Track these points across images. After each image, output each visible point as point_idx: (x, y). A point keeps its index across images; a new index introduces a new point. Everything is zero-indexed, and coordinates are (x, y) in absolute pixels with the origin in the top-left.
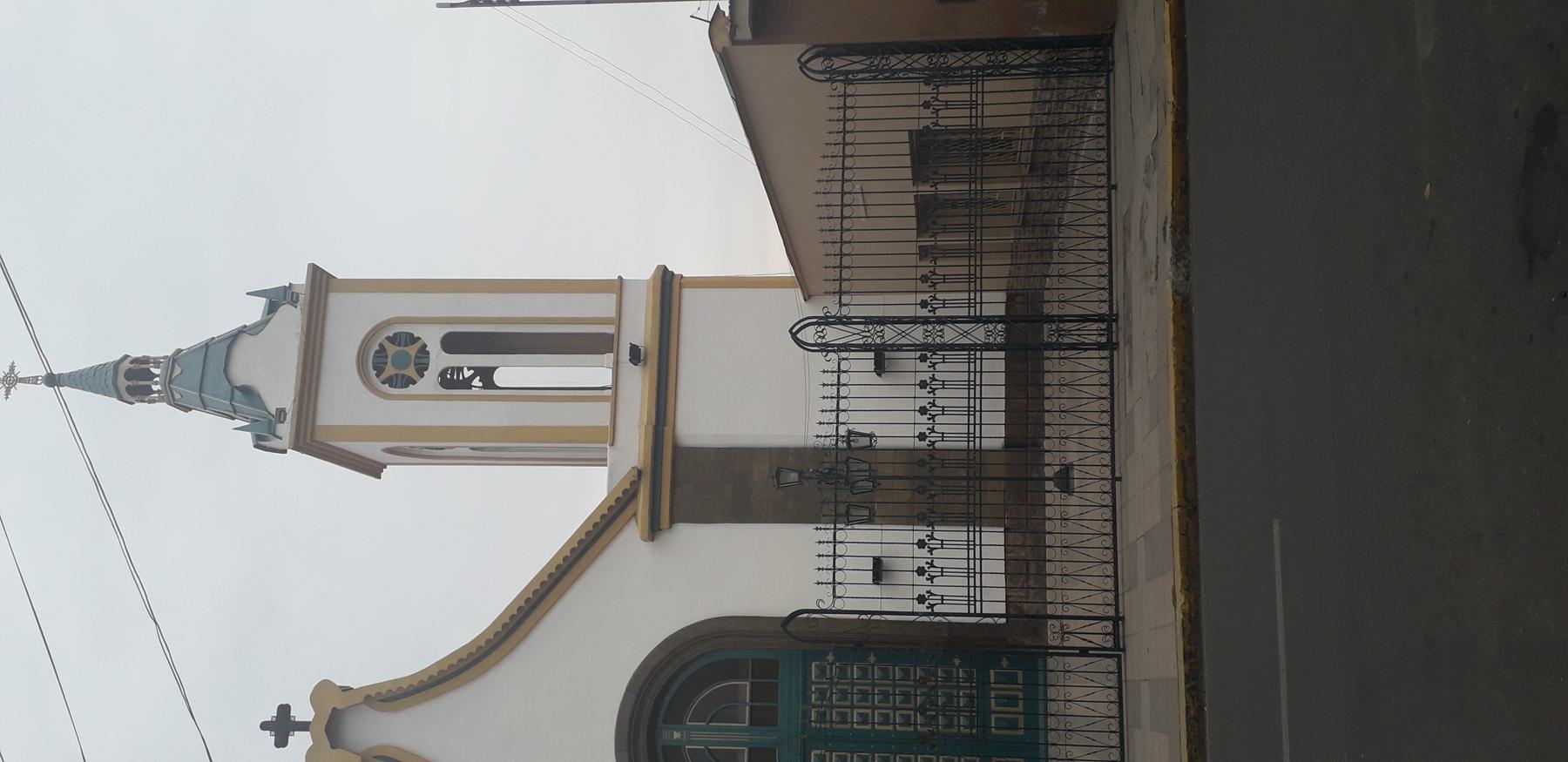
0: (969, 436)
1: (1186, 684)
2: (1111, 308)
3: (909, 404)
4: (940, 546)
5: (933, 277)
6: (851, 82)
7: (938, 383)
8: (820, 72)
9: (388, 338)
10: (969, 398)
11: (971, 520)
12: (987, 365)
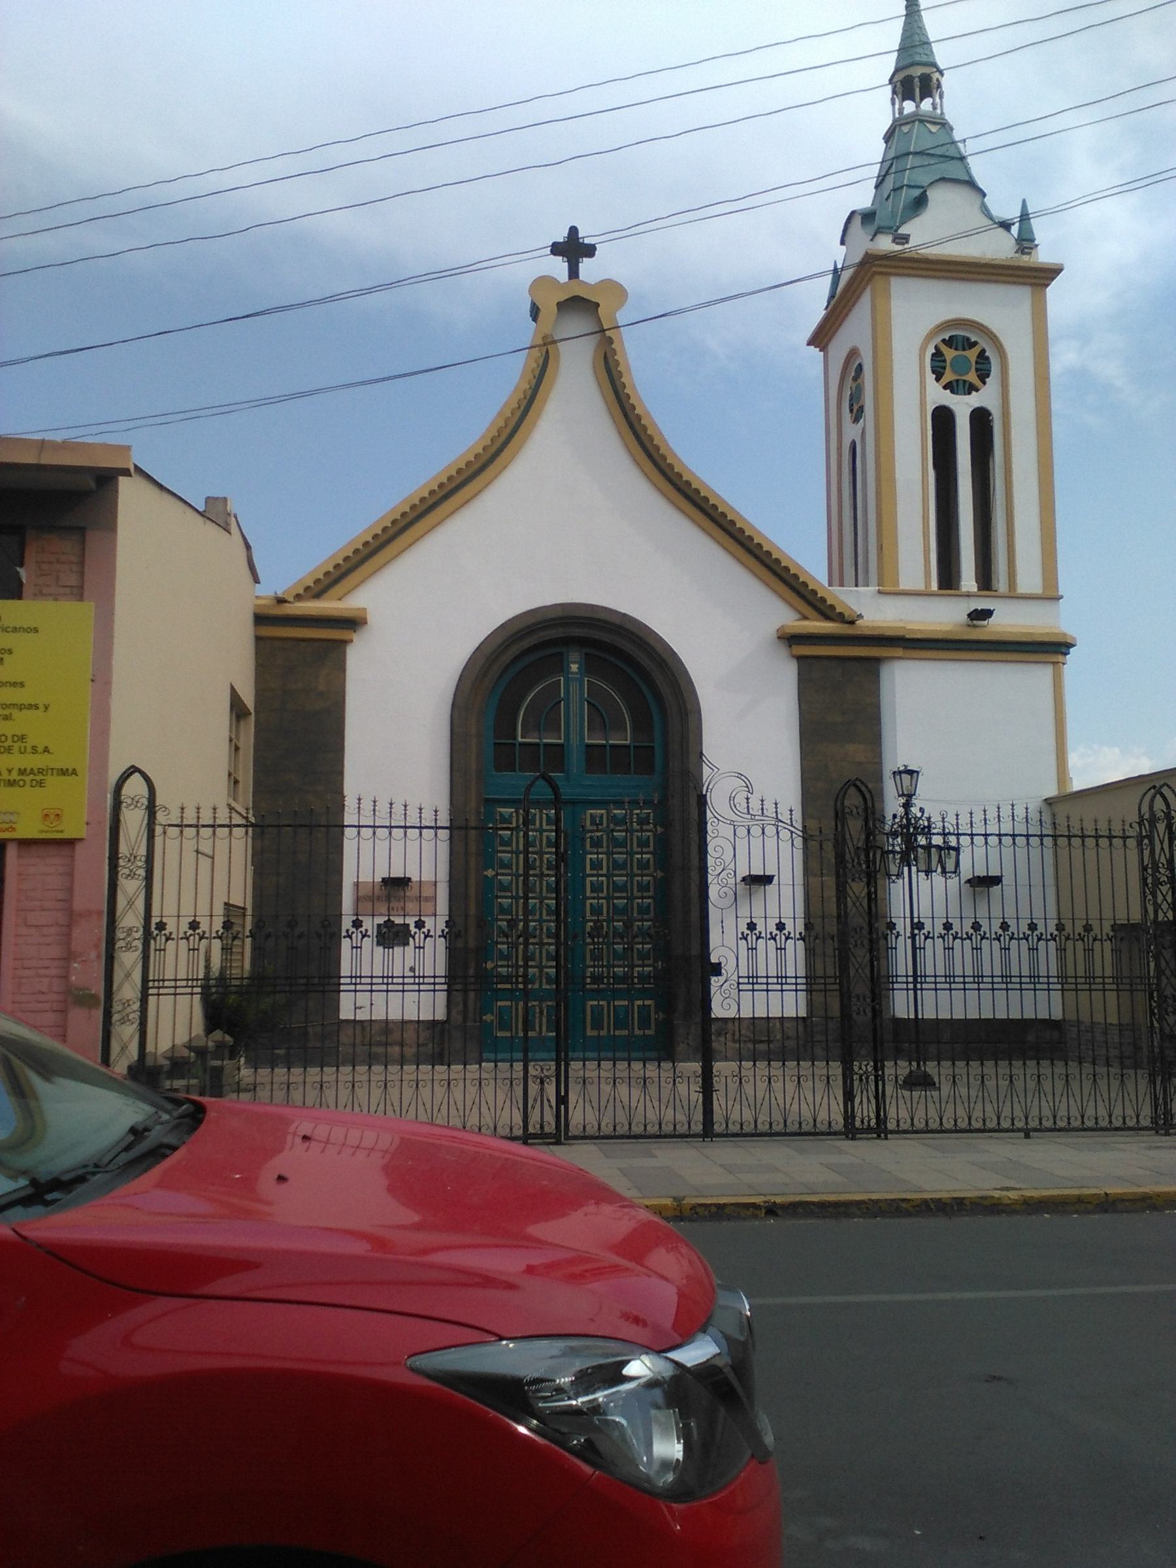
0: (356, 977)
1: (931, 1199)
2: (892, 1132)
3: (1094, 913)
4: (354, 945)
5: (1063, 937)
6: (1140, 844)
7: (1091, 942)
8: (1151, 807)
9: (983, 351)
10: (434, 977)
11: (751, 980)
12: (790, 997)
